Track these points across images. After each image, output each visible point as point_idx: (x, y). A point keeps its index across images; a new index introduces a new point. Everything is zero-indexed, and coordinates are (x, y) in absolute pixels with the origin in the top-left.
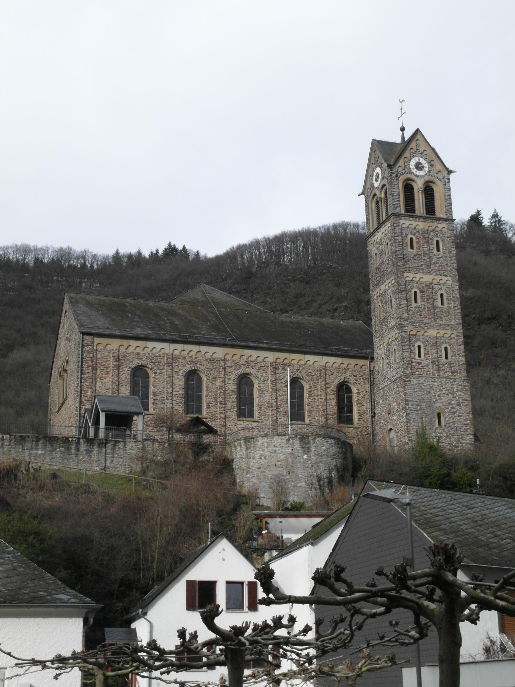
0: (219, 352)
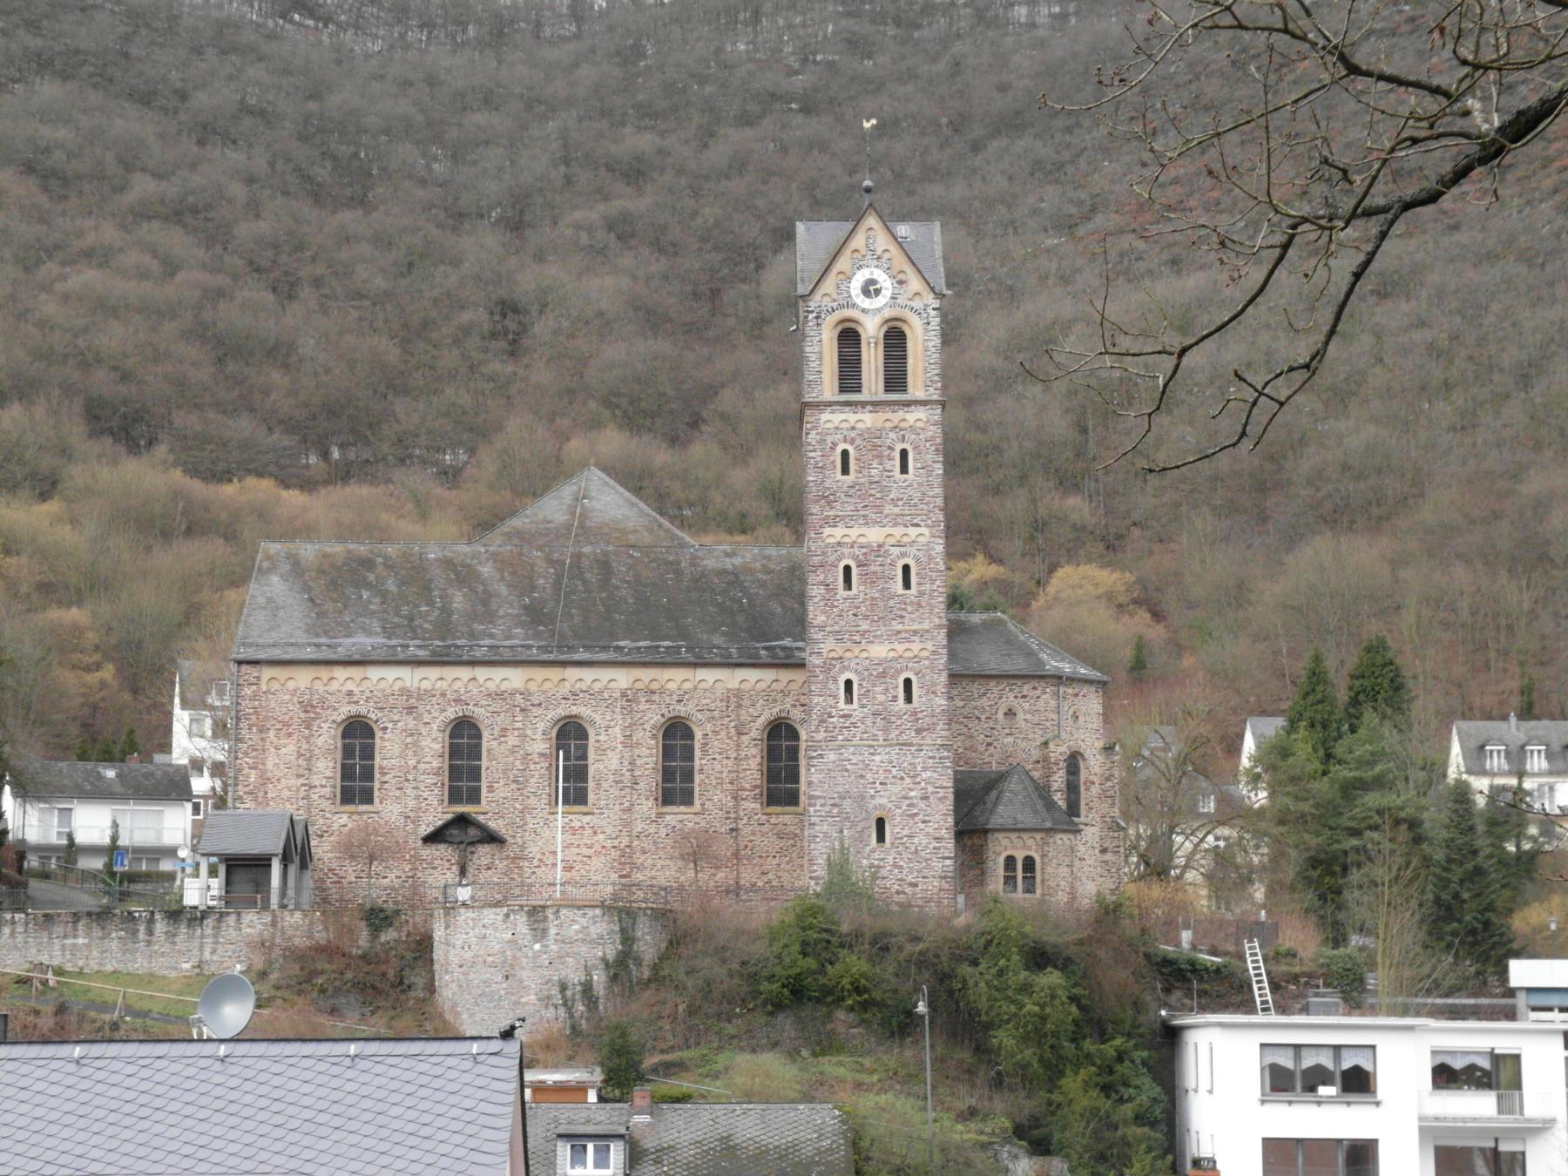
0: (515, 678)
